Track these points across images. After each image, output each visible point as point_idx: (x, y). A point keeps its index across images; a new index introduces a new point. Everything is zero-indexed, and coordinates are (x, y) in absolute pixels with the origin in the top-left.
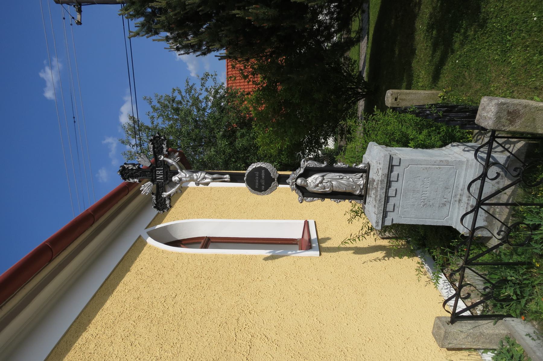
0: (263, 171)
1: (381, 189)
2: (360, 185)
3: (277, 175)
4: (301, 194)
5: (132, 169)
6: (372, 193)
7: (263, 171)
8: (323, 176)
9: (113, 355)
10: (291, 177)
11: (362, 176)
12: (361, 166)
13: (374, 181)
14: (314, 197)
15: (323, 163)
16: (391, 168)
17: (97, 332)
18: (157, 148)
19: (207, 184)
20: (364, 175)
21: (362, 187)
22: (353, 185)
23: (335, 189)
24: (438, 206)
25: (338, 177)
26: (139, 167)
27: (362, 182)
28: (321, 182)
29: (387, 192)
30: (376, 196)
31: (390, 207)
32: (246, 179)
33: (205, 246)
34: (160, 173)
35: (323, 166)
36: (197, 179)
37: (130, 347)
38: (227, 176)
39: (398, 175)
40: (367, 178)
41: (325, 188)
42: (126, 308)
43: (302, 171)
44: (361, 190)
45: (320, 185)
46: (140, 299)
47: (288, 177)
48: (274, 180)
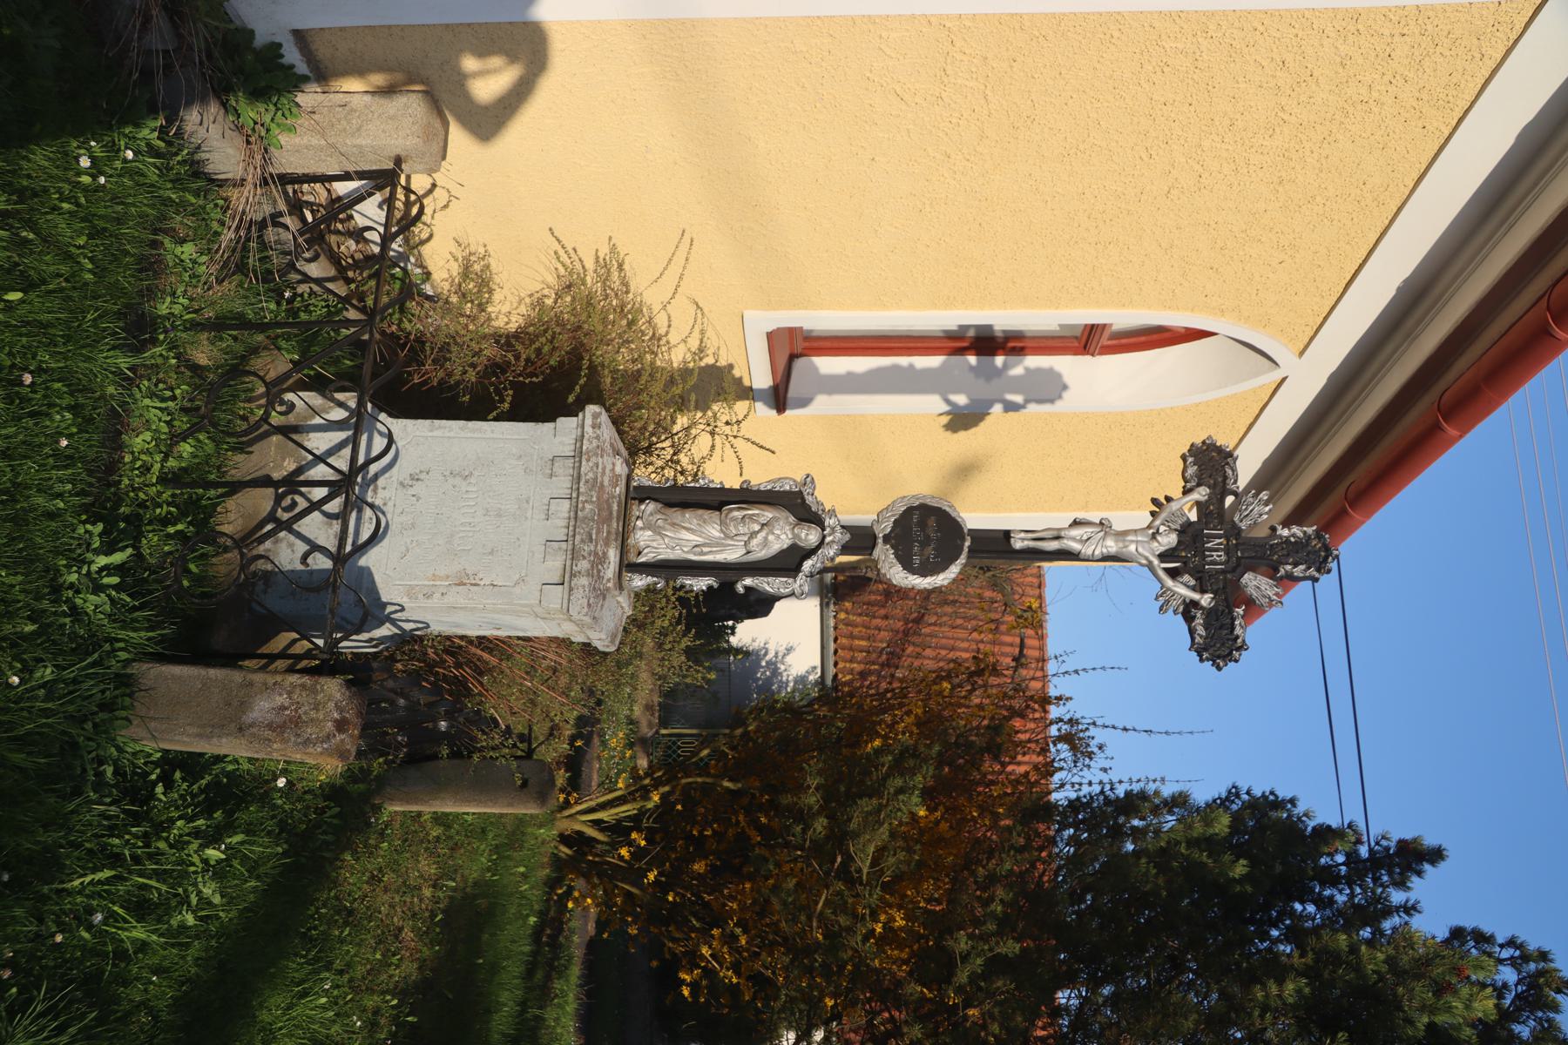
0: (932, 522)
4: (809, 499)
5: (1296, 565)
9: (1332, 35)
12: (639, 582)
15: (747, 588)
17: (1391, 89)
19: (1076, 523)
20: (633, 558)
25: (706, 550)
28: (753, 534)
32: (964, 540)
33: (1092, 330)
34: (1216, 554)
35: (748, 581)
36: (1104, 538)
37: (1289, 58)
39: (1284, 379)
40: (623, 550)
42: (1315, 155)
43: (807, 565)
45: (757, 527)
46: (1276, 180)
47: (846, 549)
48: (886, 539)
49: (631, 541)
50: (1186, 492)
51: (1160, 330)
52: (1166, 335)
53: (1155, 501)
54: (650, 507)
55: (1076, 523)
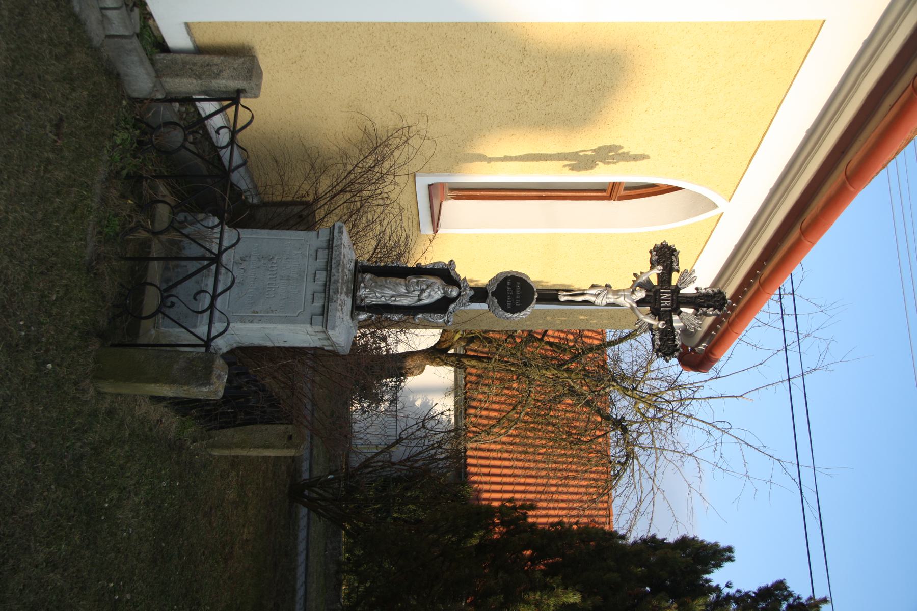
0: (509, 306)
1: (337, 281)
2: (365, 287)
3: (488, 301)
4: (452, 273)
5: (708, 307)
6: (348, 275)
7: (509, 306)
8: (420, 300)
10: (467, 298)
11: (362, 300)
13: (347, 294)
14: (432, 269)
16: (324, 312)
18: (669, 339)
19: (593, 286)
21: (362, 285)
22: (376, 287)
23: (402, 281)
24: (252, 258)
26: (697, 310)
27: (363, 292)
28: (423, 291)
29: (329, 276)
30: (343, 271)
31: (323, 255)
34: (666, 299)
36: (607, 294)
38: (562, 299)
39: (644, 157)
41: (417, 283)
44: (363, 281)
45: (424, 287)
48: (493, 294)
49: (358, 294)
50: (651, 268)
51: (653, 186)
52: (656, 189)
53: (635, 275)
54: (368, 276)
55: (593, 286)
